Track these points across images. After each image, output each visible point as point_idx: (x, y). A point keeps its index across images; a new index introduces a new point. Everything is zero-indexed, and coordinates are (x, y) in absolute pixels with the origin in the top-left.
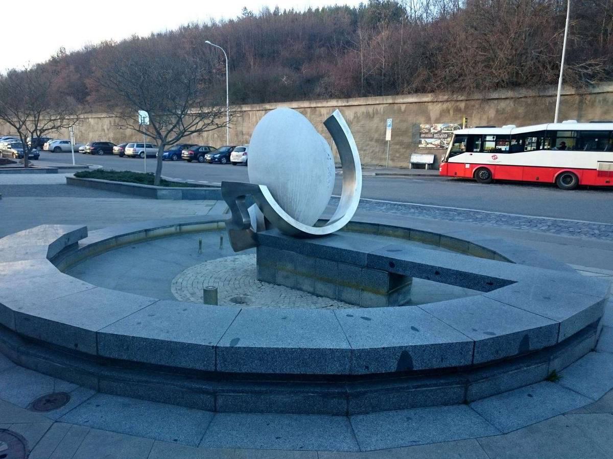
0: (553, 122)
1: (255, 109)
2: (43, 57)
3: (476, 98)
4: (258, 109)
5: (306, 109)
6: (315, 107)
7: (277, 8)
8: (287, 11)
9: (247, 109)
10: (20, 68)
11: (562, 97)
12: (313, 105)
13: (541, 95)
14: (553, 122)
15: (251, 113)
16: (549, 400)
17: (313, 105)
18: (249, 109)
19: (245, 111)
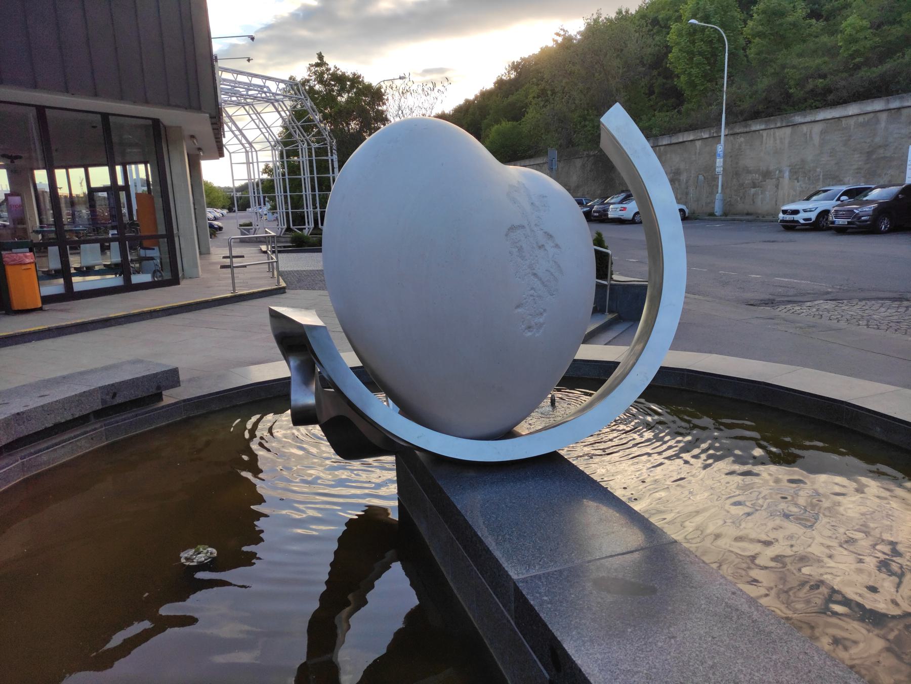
0: (597, 278)
1: (772, 126)
2: (537, 51)
3: (664, 143)
4: (779, 125)
5: (879, 114)
6: (899, 109)
7: (262, 531)
8: (260, 524)
9: (758, 127)
10: (471, 97)
11: (32, 114)
12: (895, 104)
13: (78, 208)
14: (597, 278)
15: (765, 133)
16: (283, 296)
17: (895, 104)
18: (763, 127)
19: (755, 131)
